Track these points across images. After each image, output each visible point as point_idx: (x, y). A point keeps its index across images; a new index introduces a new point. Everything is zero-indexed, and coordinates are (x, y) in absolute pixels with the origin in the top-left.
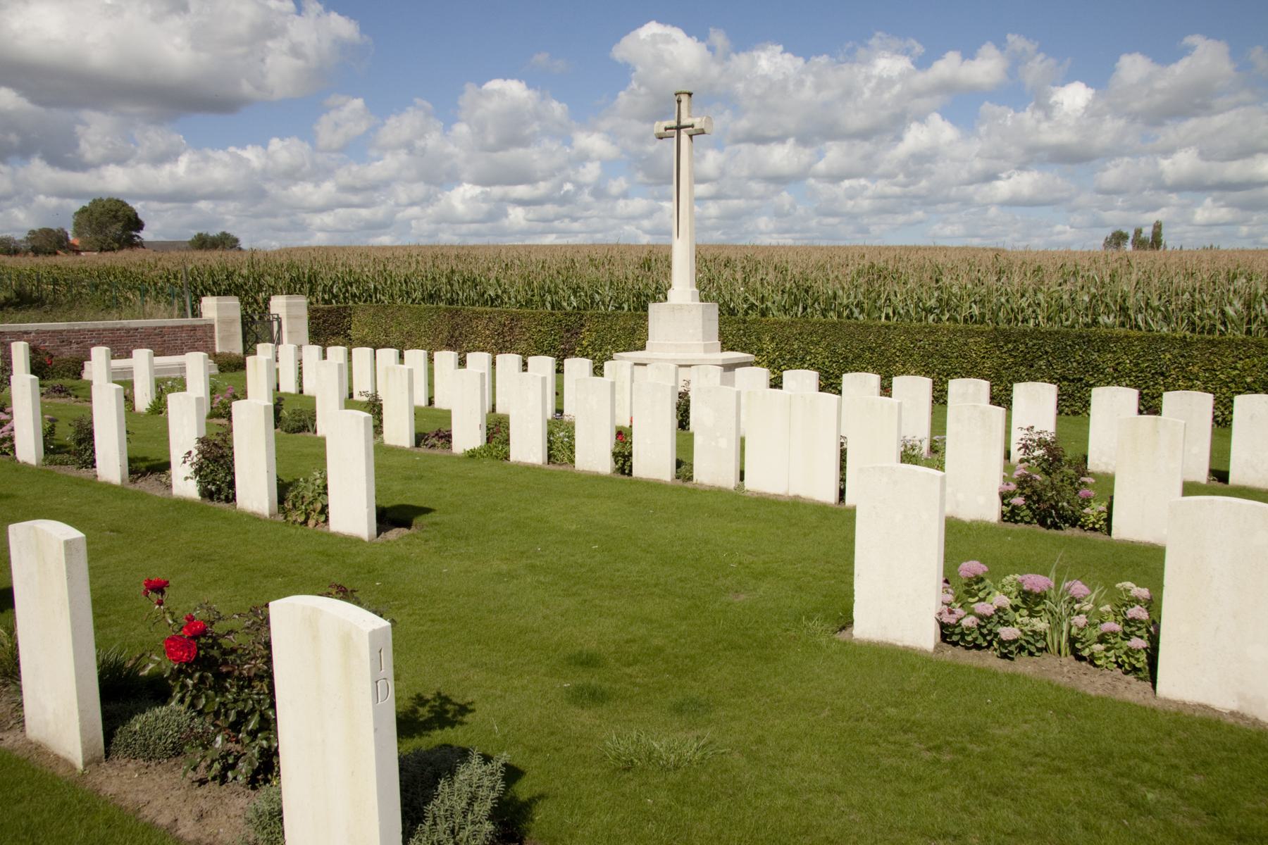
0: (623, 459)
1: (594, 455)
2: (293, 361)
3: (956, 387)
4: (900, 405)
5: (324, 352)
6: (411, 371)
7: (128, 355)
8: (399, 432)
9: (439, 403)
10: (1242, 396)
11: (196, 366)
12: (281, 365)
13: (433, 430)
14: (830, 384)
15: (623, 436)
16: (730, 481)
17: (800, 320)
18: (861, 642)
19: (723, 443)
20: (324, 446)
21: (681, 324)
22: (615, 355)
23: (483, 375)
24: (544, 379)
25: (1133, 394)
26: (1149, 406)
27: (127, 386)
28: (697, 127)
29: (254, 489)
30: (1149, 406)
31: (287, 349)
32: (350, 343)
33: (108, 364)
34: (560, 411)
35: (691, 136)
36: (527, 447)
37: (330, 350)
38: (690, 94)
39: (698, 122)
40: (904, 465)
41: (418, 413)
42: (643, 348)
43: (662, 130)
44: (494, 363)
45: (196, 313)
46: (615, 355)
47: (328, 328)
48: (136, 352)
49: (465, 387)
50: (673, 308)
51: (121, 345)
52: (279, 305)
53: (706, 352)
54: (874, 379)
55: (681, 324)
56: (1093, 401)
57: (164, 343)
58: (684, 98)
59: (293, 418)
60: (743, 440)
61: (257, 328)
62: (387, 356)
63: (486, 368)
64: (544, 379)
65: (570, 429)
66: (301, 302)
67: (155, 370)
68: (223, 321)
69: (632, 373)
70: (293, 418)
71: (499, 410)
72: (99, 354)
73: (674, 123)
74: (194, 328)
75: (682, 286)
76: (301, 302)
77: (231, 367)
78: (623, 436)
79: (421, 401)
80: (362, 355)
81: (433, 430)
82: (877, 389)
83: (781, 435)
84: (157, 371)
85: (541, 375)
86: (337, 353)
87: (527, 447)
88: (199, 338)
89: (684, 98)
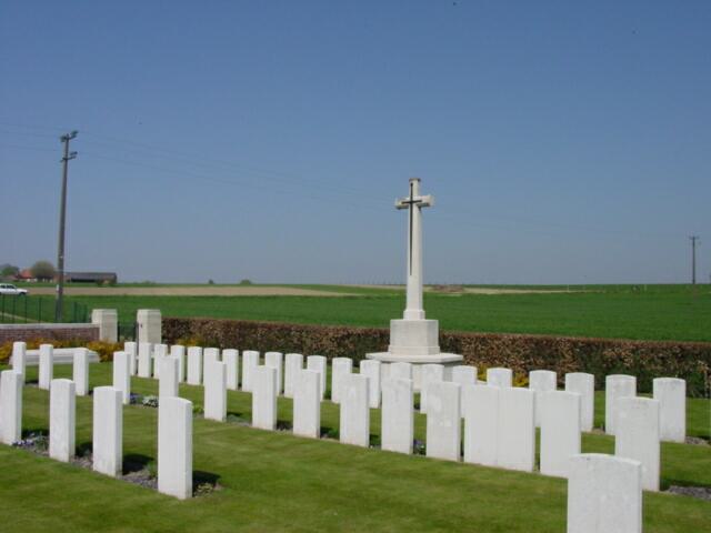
0: (284, 423)
1: (353, 431)
2: (146, 356)
3: (611, 380)
4: (535, 394)
5: (305, 360)
6: (225, 366)
7: (37, 348)
8: (215, 409)
9: (245, 388)
10: (576, 374)
11: (80, 357)
12: (140, 357)
13: (239, 407)
14: (521, 380)
15: (375, 416)
16: (453, 456)
17: (486, 334)
18: (164, 495)
19: (448, 424)
20: (47, 402)
21: (413, 332)
22: (367, 355)
23: (275, 371)
24: (319, 375)
25: (632, 380)
26: (644, 389)
27: (194, 394)
28: (424, 201)
29: (106, 457)
30: (644, 389)
31: (144, 345)
32: (187, 344)
33: (24, 353)
34: (328, 395)
35: (420, 208)
36: (306, 424)
37: (173, 347)
38: (419, 180)
39: (425, 199)
40: (179, 399)
41: (229, 394)
42: (386, 350)
43: (400, 204)
44: (186, 353)
45: (87, 319)
46: (367, 355)
47: (174, 332)
48: (42, 346)
49: (216, 369)
50: (408, 325)
51: (33, 341)
52: (143, 315)
53: (430, 354)
54: (552, 376)
55: (413, 332)
56: (115, 358)
57: (61, 340)
58: (415, 183)
59: (142, 400)
60: (463, 421)
61: (128, 331)
62: (212, 352)
63: (278, 366)
64: (319, 375)
65: (337, 409)
66: (157, 314)
67: (53, 358)
68: (105, 326)
69: (380, 369)
70: (142, 400)
71: (287, 395)
72: (18, 346)
73: (408, 199)
74: (85, 330)
75: (414, 310)
76: (157, 314)
77: (106, 356)
78: (375, 416)
79: (233, 385)
80: (194, 351)
81: (239, 407)
82: (554, 384)
83: (503, 421)
84: (55, 359)
85: (317, 372)
86: (178, 349)
87: (306, 424)
88: (86, 339)
89: (415, 183)
